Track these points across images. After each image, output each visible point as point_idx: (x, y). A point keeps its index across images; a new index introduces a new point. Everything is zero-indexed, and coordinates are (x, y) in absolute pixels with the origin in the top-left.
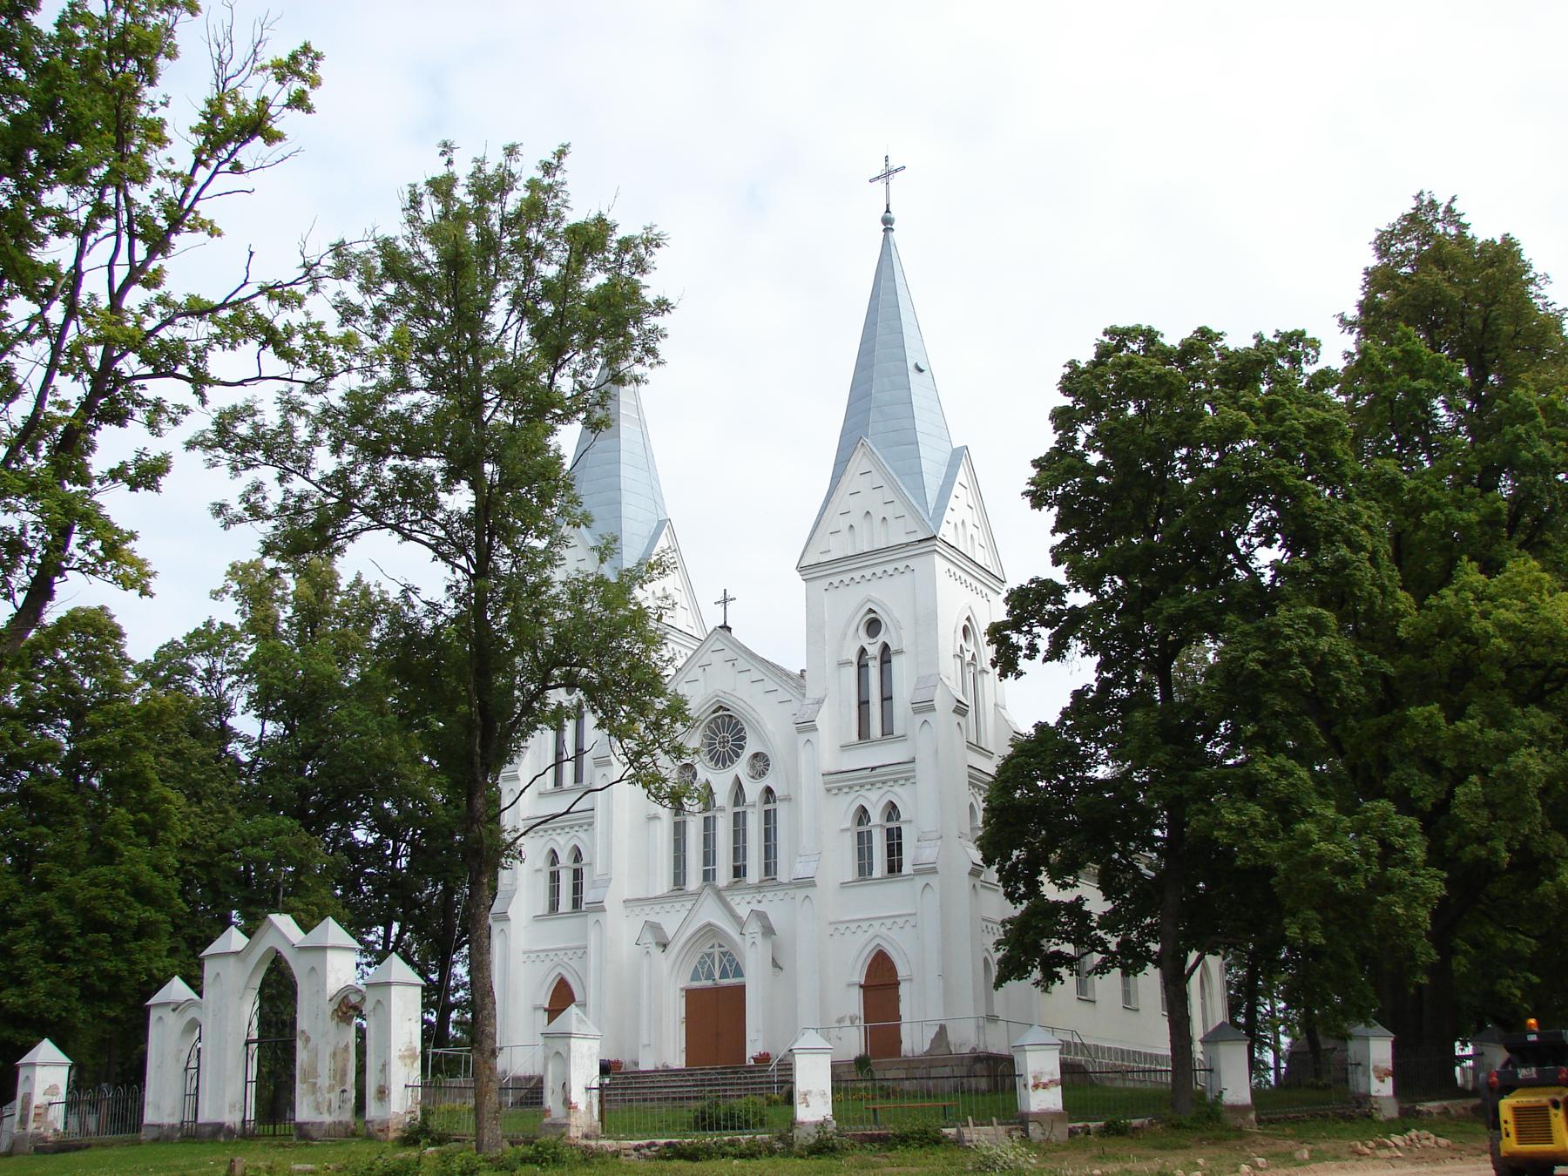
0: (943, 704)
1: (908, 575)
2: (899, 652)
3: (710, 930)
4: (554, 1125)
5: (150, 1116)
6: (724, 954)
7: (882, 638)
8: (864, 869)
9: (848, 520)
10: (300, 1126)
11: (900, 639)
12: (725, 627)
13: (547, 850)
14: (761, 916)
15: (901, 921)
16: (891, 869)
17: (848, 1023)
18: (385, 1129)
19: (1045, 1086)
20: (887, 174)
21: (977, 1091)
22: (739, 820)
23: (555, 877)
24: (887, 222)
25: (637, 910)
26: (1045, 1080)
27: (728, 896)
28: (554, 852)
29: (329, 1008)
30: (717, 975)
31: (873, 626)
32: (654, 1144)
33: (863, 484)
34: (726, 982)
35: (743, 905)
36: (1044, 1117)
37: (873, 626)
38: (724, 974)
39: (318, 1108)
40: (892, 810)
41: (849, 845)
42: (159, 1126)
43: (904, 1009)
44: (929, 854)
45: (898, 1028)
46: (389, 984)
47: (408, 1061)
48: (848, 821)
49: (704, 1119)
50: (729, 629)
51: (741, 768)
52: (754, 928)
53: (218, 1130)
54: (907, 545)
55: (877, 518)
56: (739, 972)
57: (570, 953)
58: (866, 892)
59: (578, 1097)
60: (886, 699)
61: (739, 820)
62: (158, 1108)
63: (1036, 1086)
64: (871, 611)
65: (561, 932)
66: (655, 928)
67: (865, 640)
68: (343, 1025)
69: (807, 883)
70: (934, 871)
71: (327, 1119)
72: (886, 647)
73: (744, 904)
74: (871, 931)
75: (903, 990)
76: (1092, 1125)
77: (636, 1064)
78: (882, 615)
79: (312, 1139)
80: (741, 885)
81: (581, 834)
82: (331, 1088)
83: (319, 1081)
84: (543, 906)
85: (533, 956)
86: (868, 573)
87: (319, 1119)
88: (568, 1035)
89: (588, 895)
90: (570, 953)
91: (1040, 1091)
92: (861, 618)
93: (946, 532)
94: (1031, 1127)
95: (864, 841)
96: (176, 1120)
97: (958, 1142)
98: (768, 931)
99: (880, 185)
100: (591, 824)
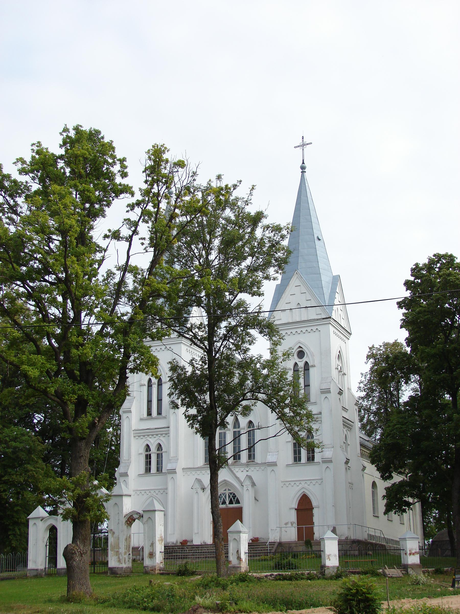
0: (334, 391)
1: (317, 333)
4: (234, 567)
5: (31, 565)
6: (231, 493)
7: (305, 359)
10: (111, 569)
11: (314, 361)
14: (250, 477)
15: (314, 482)
16: (308, 459)
17: (290, 525)
18: (153, 569)
19: (413, 554)
20: (303, 145)
21: (354, 555)
23: (148, 457)
24: (303, 168)
25: (193, 473)
26: (413, 552)
28: (148, 446)
29: (124, 520)
30: (227, 502)
32: (273, 575)
33: (297, 291)
34: (231, 506)
36: (413, 566)
38: (231, 502)
39: (119, 561)
42: (37, 570)
43: (315, 519)
44: (328, 454)
45: (312, 528)
46: (155, 511)
47: (161, 542)
49: (279, 565)
52: (247, 483)
54: (318, 320)
56: (238, 502)
57: (157, 491)
59: (244, 557)
62: (35, 562)
63: (410, 554)
64: (300, 347)
65: (153, 481)
67: (297, 360)
68: (129, 527)
69: (274, 464)
70: (331, 461)
71: (124, 566)
72: (306, 363)
73: (240, 471)
74: (300, 486)
75: (315, 511)
76: (430, 570)
77: (192, 541)
78: (305, 349)
79: (117, 574)
80: (237, 463)
81: (162, 438)
82: (125, 553)
83: (120, 550)
85: (138, 492)
86: (299, 330)
87: (121, 566)
88: (240, 532)
89: (166, 466)
90: (157, 491)
91: (412, 556)
93: (333, 317)
94: (409, 570)
96: (42, 567)
97: (385, 575)
98: (253, 484)
99: (299, 150)
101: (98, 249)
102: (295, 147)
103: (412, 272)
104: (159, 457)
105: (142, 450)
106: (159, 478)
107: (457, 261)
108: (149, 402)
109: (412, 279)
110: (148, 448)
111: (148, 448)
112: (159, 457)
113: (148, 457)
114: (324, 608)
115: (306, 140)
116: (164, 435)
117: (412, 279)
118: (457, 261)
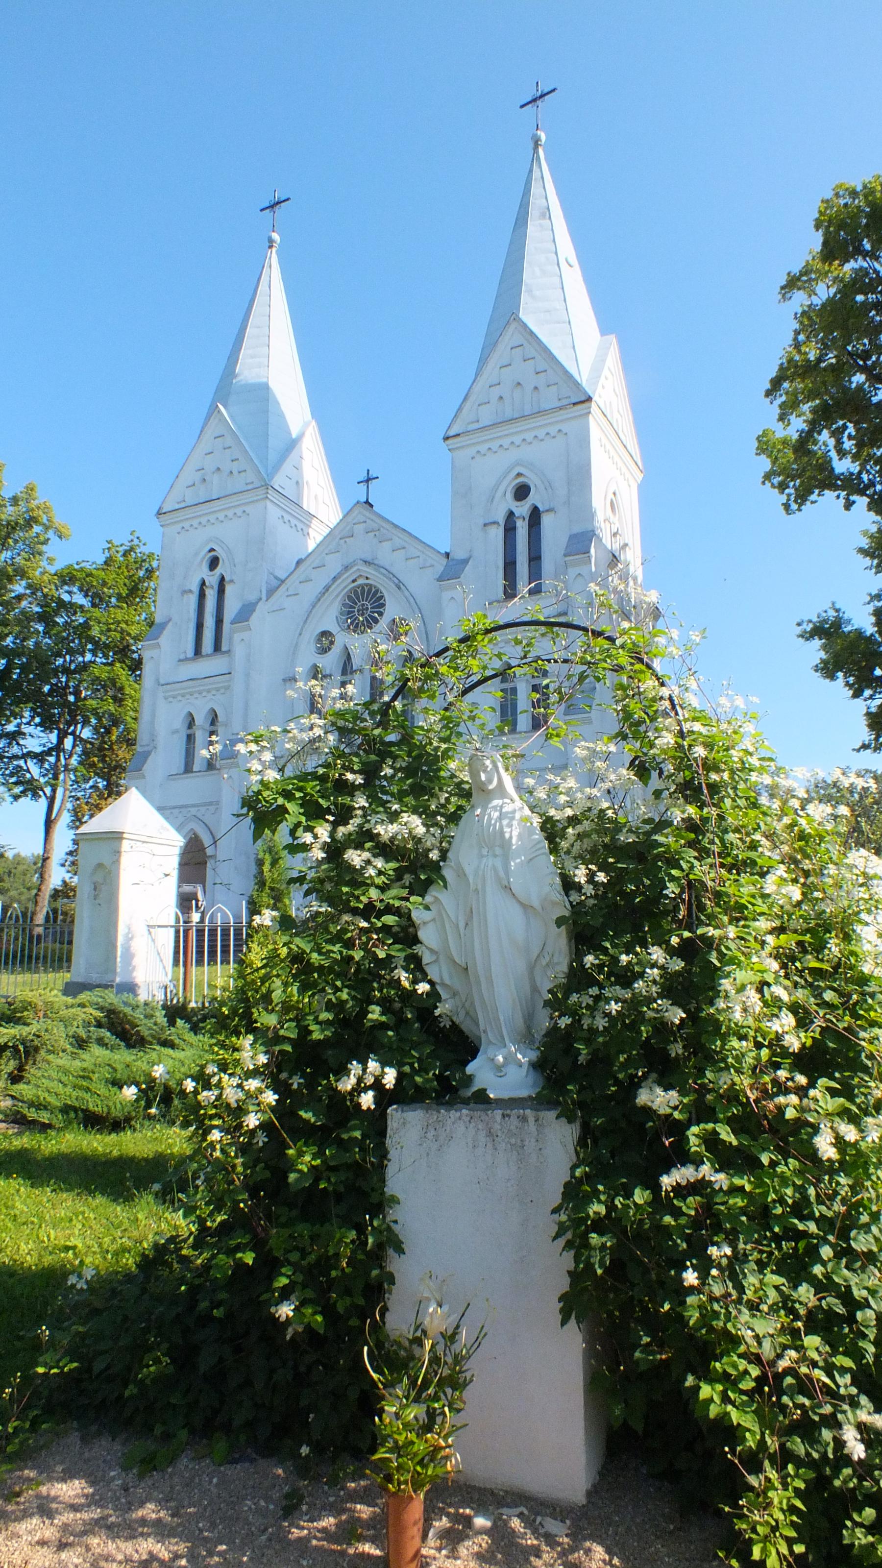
2: (232, 581)
9: (496, 392)
13: (185, 711)
20: (368, 480)
28: (191, 714)
31: (214, 563)
50: (371, 506)
55: (235, 472)
60: (219, 622)
64: (212, 550)
67: (204, 572)
72: (222, 579)
78: (220, 553)
92: (509, 485)
100: (227, 688)
105: (179, 723)
106: (209, 779)
107: (879, 772)
108: (199, 627)
110: (191, 722)
111: (191, 722)
114: (568, 1260)
115: (373, 474)
116: (222, 691)
118: (879, 772)
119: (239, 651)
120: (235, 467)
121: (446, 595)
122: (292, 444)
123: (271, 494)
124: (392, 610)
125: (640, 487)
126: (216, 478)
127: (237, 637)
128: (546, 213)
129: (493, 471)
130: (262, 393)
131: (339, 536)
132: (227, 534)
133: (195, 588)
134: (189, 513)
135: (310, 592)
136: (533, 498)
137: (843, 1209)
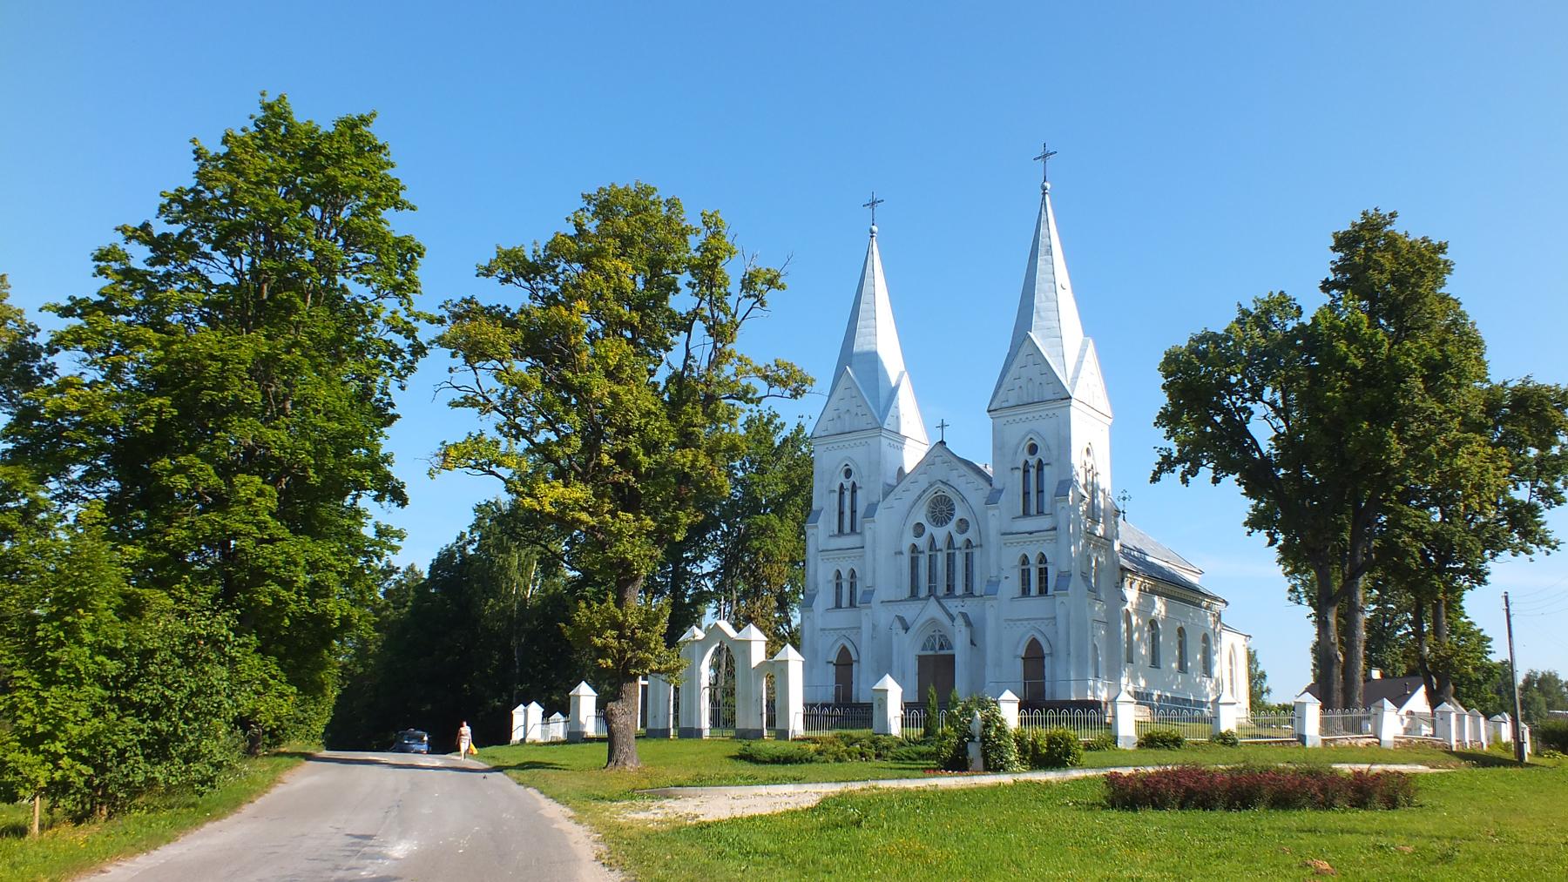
3: (933, 621)
8: (1026, 592)
12: (942, 443)
14: (965, 615)
22: (950, 559)
23: (839, 586)
27: (943, 601)
35: (954, 606)
37: (1033, 449)
38: (942, 647)
40: (1043, 559)
41: (832, 589)
48: (1017, 561)
51: (951, 526)
52: (960, 621)
53: (533, 743)
56: (951, 647)
58: (1027, 602)
60: (853, 512)
61: (950, 559)
66: (901, 619)
67: (842, 479)
78: (851, 466)
84: (832, 603)
92: (1026, 444)
95: (1025, 574)
101: (84, 752)
102: (1155, 479)
103: (1192, 350)
104: (852, 586)
105: (832, 576)
108: (841, 513)
109: (1520, 680)
110: (839, 575)
111: (839, 575)
112: (852, 586)
113: (839, 586)
117: (1520, 680)
119: (868, 534)
120: (859, 411)
121: (990, 513)
122: (894, 391)
123: (884, 433)
124: (959, 513)
125: (1111, 428)
126: (847, 417)
127: (867, 526)
128: (1049, 251)
129: (1018, 432)
130: (872, 358)
131: (926, 463)
132: (854, 453)
133: (837, 488)
134: (830, 440)
135: (910, 497)
136: (1039, 455)
137: (368, 532)
